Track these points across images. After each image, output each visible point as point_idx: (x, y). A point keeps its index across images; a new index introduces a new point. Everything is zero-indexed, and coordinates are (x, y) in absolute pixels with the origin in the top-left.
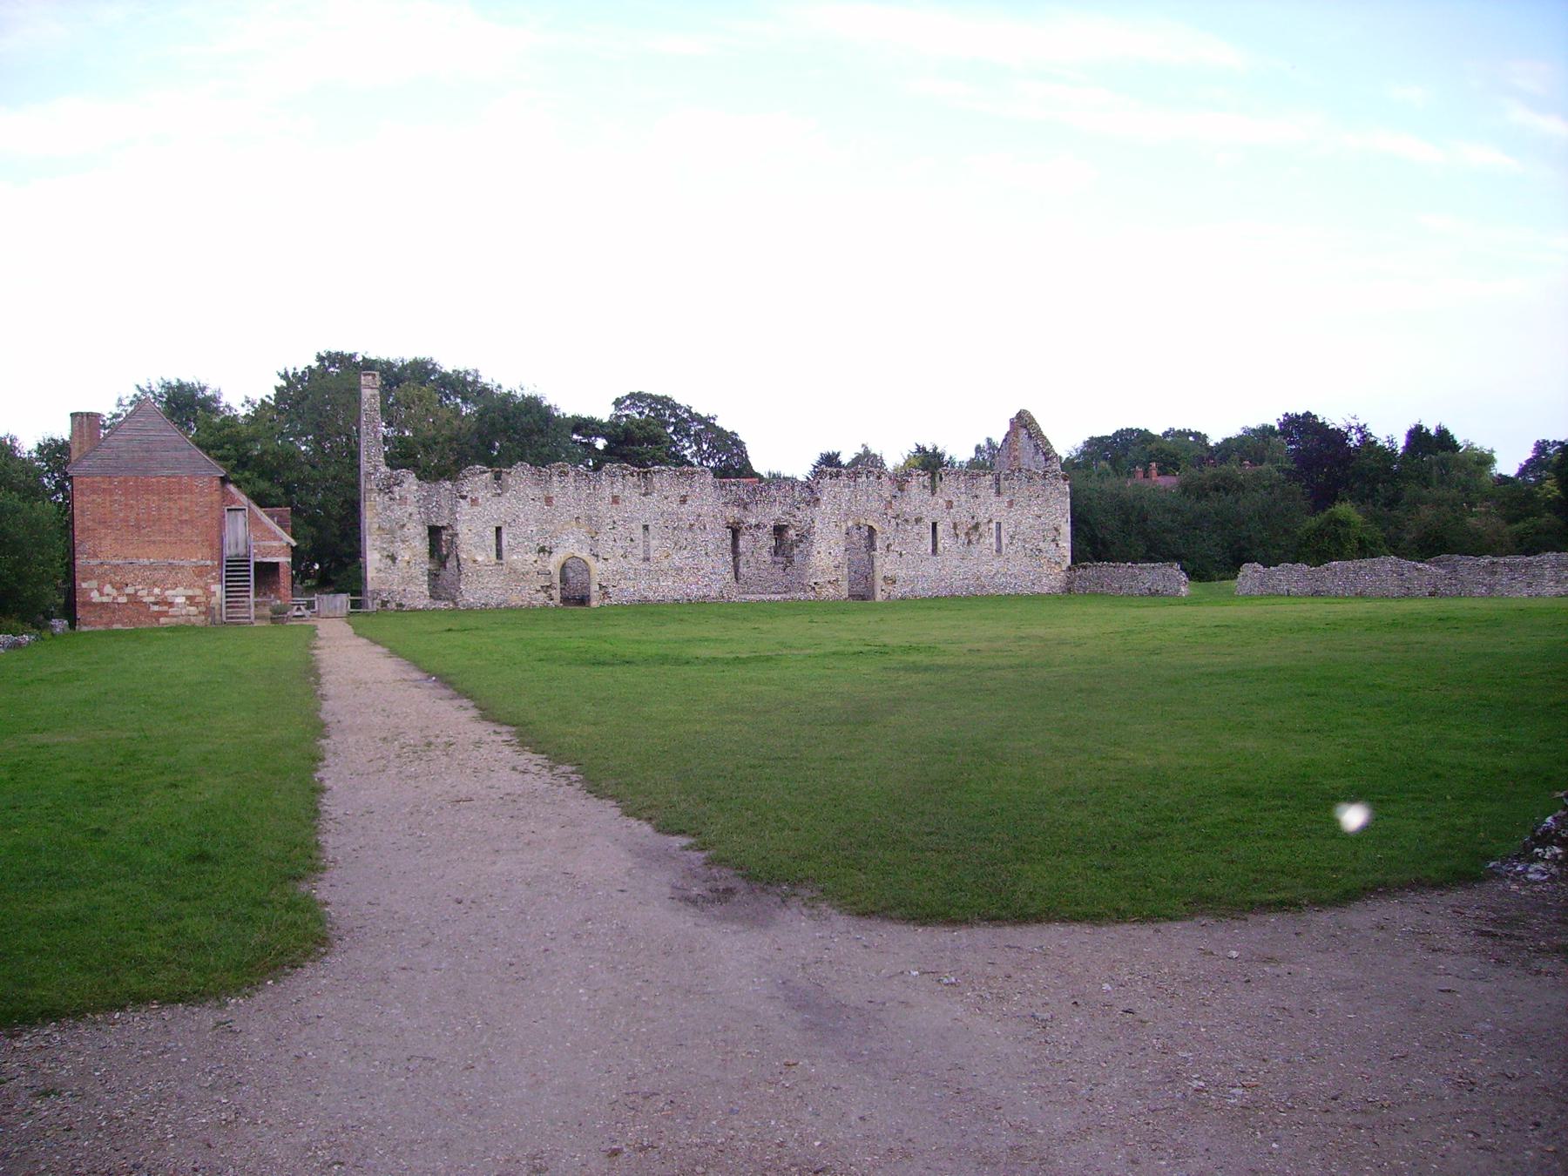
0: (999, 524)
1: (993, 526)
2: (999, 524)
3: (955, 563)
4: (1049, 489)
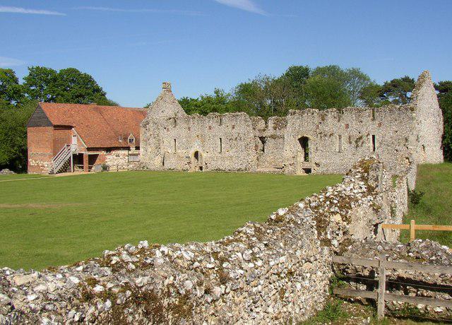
0: (374, 137)
1: (371, 137)
2: (374, 137)
3: (350, 156)
4: (402, 116)
